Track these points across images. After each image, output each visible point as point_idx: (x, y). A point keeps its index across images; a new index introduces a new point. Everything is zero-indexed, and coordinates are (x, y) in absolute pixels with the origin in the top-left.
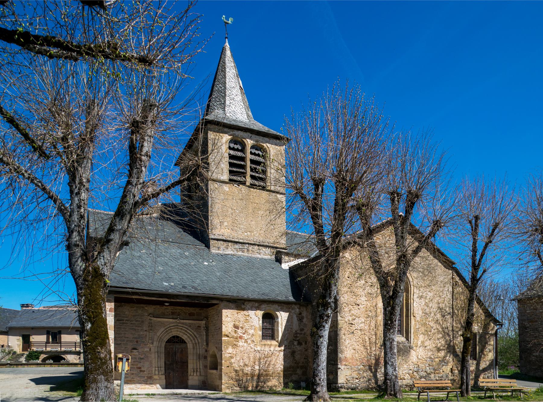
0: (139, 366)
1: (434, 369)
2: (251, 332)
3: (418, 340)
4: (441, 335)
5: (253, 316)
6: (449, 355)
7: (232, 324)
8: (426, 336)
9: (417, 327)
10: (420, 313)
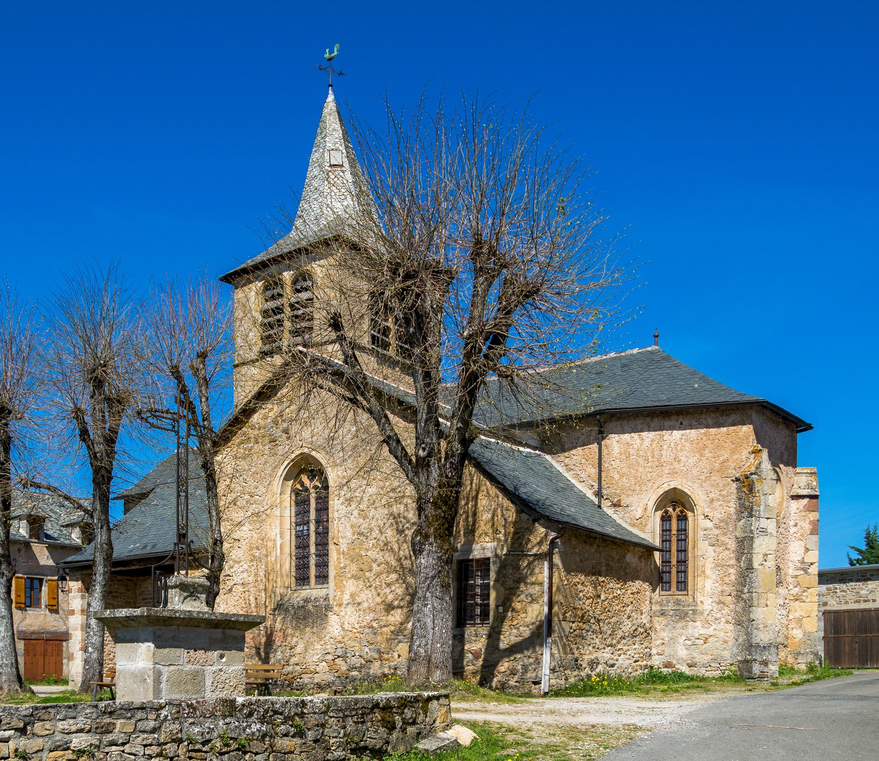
1: (379, 652)
3: (342, 592)
8: (361, 583)
10: (349, 534)
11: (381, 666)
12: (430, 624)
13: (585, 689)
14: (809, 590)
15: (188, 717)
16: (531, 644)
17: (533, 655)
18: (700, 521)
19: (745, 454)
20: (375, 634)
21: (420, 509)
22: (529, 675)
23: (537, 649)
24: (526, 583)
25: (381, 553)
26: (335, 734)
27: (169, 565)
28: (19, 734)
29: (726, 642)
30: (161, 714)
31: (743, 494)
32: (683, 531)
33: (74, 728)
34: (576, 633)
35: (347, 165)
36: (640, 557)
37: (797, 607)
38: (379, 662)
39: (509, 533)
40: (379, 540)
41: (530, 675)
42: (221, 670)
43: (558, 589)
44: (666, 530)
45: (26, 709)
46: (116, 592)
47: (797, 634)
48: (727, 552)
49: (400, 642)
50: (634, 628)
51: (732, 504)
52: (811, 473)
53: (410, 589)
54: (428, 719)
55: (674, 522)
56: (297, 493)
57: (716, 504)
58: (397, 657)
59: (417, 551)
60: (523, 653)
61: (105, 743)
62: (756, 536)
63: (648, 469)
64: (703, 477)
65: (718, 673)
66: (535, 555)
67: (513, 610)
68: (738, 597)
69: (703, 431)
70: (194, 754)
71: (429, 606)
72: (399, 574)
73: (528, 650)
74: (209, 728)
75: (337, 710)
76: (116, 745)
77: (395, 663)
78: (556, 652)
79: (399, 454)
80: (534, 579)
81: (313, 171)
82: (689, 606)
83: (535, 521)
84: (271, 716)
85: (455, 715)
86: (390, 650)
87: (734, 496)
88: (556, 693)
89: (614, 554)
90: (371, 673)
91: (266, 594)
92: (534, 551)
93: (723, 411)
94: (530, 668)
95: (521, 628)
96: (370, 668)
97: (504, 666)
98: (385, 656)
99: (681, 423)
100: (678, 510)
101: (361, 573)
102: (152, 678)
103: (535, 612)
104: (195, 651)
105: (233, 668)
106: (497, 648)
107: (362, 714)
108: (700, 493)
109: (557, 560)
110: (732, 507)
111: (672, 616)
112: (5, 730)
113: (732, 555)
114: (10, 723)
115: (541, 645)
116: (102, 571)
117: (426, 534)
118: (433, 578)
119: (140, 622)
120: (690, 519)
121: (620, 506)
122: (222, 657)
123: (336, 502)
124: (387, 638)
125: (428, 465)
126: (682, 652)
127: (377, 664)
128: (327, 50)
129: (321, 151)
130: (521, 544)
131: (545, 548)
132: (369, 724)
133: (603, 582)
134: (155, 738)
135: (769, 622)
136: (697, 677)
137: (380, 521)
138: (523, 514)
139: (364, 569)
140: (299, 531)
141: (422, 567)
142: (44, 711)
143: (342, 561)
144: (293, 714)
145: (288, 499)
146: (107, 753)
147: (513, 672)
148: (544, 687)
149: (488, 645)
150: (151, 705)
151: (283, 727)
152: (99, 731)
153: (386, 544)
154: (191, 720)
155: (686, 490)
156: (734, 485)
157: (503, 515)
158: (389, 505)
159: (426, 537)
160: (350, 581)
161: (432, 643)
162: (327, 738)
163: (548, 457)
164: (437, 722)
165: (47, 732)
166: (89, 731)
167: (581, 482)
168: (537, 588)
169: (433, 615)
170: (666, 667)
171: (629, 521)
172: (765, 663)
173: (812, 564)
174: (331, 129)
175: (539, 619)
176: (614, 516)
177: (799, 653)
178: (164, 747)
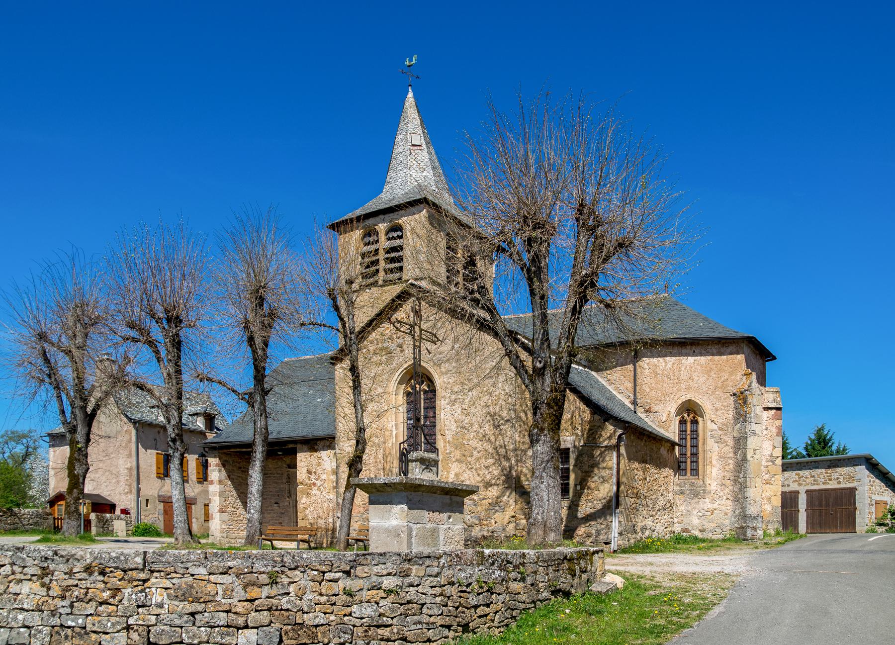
0: (280, 521)
1: (480, 519)
2: (324, 477)
3: (448, 472)
4: (491, 461)
5: (326, 458)
6: (507, 494)
7: (306, 469)
8: (464, 465)
9: (448, 451)
10: (453, 427)
11: (481, 530)
12: (545, 497)
13: (643, 547)
14: (776, 476)
15: (457, 565)
16: (603, 514)
17: (604, 522)
18: (708, 425)
19: (739, 376)
20: (476, 505)
21: (535, 409)
22: (601, 537)
23: (608, 518)
24: (599, 468)
25: (480, 443)
26: (543, 580)
27: (292, 448)
28: (346, 576)
29: (726, 514)
30: (441, 562)
31: (739, 405)
32: (695, 432)
33: (385, 572)
34: (633, 506)
35: (424, 146)
36: (668, 451)
37: (767, 489)
38: (479, 527)
39: (585, 429)
40: (478, 432)
41: (602, 537)
42: (449, 528)
43: (624, 473)
44: (683, 431)
45: (351, 555)
46: (244, 468)
47: (768, 508)
48: (727, 448)
49: (496, 511)
50: (665, 503)
51: (731, 412)
52: (776, 392)
53: (504, 471)
54: (593, 568)
55: (689, 425)
56: (408, 394)
57: (720, 412)
58: (494, 523)
59: (533, 442)
60: (596, 521)
61: (406, 584)
62: (749, 436)
63: (670, 385)
64: (710, 392)
65: (721, 537)
66: (606, 447)
67: (589, 488)
68: (736, 481)
69: (709, 358)
70: (462, 595)
71: (545, 483)
72: (496, 459)
73: (601, 519)
74: (470, 574)
75: (543, 561)
76: (413, 586)
77: (493, 527)
78: (623, 520)
79: (518, 365)
80: (604, 465)
81: (398, 148)
82: (700, 487)
83: (606, 420)
84: (505, 565)
85: (607, 567)
86: (489, 517)
87: (732, 407)
88: (625, 551)
89: (654, 448)
90: (473, 535)
91: (384, 473)
92: (605, 444)
93: (723, 343)
94: (602, 532)
95: (595, 502)
96: (472, 531)
97: (581, 531)
98: (485, 522)
99: (694, 352)
100: (691, 416)
101: (464, 458)
102: (406, 534)
103: (606, 490)
104: (433, 512)
105: (456, 527)
106: (576, 517)
107: (558, 564)
108: (708, 404)
109: (623, 450)
110: (731, 414)
111: (688, 495)
112: (335, 572)
113: (731, 450)
114: (339, 567)
115: (611, 515)
116: (261, 450)
117: (542, 427)
118: (548, 461)
119: (396, 488)
120: (701, 423)
121: (650, 412)
122: (449, 518)
123: (443, 402)
124: (486, 509)
125: (544, 375)
126: (696, 521)
127: (478, 528)
128: (407, 59)
129: (404, 133)
130: (594, 438)
131: (614, 441)
132: (561, 572)
133: (648, 468)
134: (438, 581)
135: (757, 499)
136: (707, 539)
137: (479, 418)
138: (596, 415)
139: (466, 454)
140: (410, 424)
141: (539, 453)
142: (363, 557)
143: (448, 448)
144: (518, 563)
145: (401, 399)
146: (407, 592)
147: (589, 535)
148: (613, 546)
149: (568, 515)
150: (434, 555)
151: (513, 574)
152: (402, 575)
153: (484, 436)
154: (459, 567)
155: (698, 401)
156: (732, 398)
157: (580, 416)
158: (487, 406)
159: (542, 430)
160: (455, 464)
161: (548, 512)
162: (538, 582)
163: (594, 373)
164: (598, 570)
165: (366, 575)
166: (395, 575)
167: (620, 393)
168: (608, 471)
169: (548, 490)
170: (684, 532)
171: (657, 423)
172: (755, 529)
173: (777, 457)
174: (411, 118)
175: (609, 495)
176: (646, 420)
177: (769, 522)
178: (443, 588)
